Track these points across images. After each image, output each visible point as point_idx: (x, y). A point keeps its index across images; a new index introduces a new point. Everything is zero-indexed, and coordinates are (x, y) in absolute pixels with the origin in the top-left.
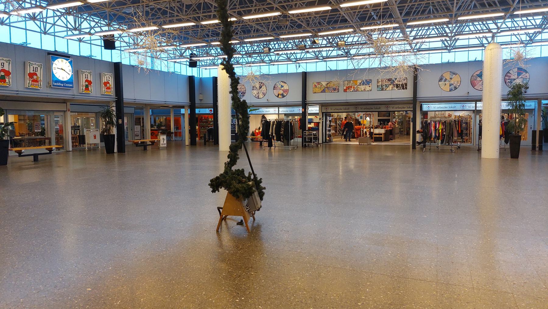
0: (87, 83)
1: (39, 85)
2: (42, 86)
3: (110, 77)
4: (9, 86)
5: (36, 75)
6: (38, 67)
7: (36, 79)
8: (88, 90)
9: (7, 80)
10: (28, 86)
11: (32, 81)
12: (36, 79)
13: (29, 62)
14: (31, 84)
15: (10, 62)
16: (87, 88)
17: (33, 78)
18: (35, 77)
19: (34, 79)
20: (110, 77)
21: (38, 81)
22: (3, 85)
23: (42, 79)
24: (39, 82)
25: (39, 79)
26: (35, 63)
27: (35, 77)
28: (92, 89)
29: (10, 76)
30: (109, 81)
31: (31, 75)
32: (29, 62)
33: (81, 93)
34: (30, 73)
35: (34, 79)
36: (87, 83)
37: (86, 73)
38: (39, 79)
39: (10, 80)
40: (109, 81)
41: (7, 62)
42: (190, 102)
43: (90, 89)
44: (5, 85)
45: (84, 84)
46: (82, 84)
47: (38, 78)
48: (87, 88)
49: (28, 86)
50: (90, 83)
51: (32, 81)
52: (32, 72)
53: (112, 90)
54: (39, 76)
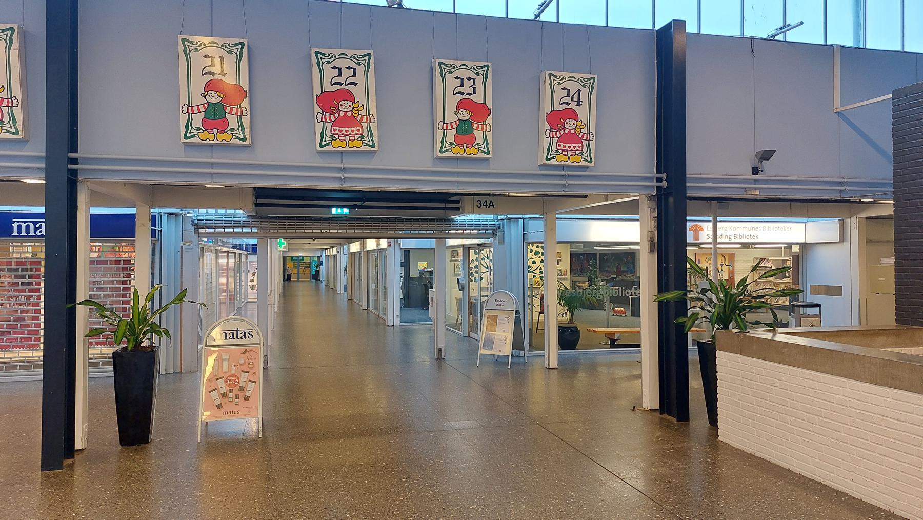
0: (465, 115)
1: (365, 134)
2: (593, 152)
3: (354, 65)
4: (485, 156)
5: (350, 96)
6: (581, 88)
7: (573, 131)
8: (222, 130)
9: (478, 135)
10: (441, 152)
11: (334, 123)
12: (573, 131)
13: (317, 53)
14: (332, 137)
15: (369, 65)
16: (464, 131)
17: (564, 128)
18: (570, 124)
19: (567, 131)
20: (360, 70)
21: (361, 121)
22: (465, 155)
23: (373, 111)
24: (585, 142)
25: (585, 131)
26: (343, 51)
27: (570, 124)
28: (592, 148)
29: (489, 120)
30: (350, 87)
31: (557, 119)
32: (317, 53)
33: (543, 166)
34: (552, 111)
35: (342, 114)
36: (465, 115)
37: (464, 74)
38: (585, 131)
39: (490, 136)
40: (350, 87)
41: (230, 53)
42: (659, 171)
43: (479, 138)
44: (472, 153)
45: (451, 118)
46: (184, 100)
47: (356, 109)
48: (464, 131)
49: (441, 152)
50: (480, 111)
51: (334, 123)
52: (558, 107)
53: (588, 146)
54: (363, 101)
